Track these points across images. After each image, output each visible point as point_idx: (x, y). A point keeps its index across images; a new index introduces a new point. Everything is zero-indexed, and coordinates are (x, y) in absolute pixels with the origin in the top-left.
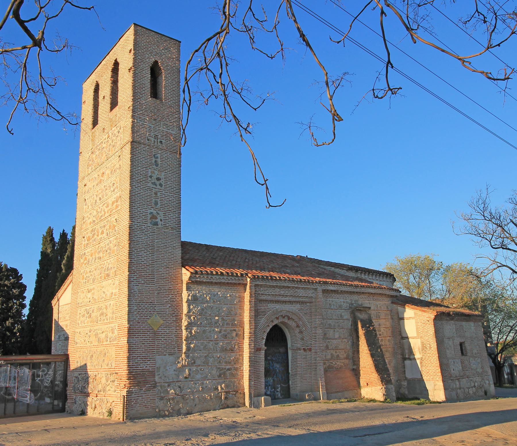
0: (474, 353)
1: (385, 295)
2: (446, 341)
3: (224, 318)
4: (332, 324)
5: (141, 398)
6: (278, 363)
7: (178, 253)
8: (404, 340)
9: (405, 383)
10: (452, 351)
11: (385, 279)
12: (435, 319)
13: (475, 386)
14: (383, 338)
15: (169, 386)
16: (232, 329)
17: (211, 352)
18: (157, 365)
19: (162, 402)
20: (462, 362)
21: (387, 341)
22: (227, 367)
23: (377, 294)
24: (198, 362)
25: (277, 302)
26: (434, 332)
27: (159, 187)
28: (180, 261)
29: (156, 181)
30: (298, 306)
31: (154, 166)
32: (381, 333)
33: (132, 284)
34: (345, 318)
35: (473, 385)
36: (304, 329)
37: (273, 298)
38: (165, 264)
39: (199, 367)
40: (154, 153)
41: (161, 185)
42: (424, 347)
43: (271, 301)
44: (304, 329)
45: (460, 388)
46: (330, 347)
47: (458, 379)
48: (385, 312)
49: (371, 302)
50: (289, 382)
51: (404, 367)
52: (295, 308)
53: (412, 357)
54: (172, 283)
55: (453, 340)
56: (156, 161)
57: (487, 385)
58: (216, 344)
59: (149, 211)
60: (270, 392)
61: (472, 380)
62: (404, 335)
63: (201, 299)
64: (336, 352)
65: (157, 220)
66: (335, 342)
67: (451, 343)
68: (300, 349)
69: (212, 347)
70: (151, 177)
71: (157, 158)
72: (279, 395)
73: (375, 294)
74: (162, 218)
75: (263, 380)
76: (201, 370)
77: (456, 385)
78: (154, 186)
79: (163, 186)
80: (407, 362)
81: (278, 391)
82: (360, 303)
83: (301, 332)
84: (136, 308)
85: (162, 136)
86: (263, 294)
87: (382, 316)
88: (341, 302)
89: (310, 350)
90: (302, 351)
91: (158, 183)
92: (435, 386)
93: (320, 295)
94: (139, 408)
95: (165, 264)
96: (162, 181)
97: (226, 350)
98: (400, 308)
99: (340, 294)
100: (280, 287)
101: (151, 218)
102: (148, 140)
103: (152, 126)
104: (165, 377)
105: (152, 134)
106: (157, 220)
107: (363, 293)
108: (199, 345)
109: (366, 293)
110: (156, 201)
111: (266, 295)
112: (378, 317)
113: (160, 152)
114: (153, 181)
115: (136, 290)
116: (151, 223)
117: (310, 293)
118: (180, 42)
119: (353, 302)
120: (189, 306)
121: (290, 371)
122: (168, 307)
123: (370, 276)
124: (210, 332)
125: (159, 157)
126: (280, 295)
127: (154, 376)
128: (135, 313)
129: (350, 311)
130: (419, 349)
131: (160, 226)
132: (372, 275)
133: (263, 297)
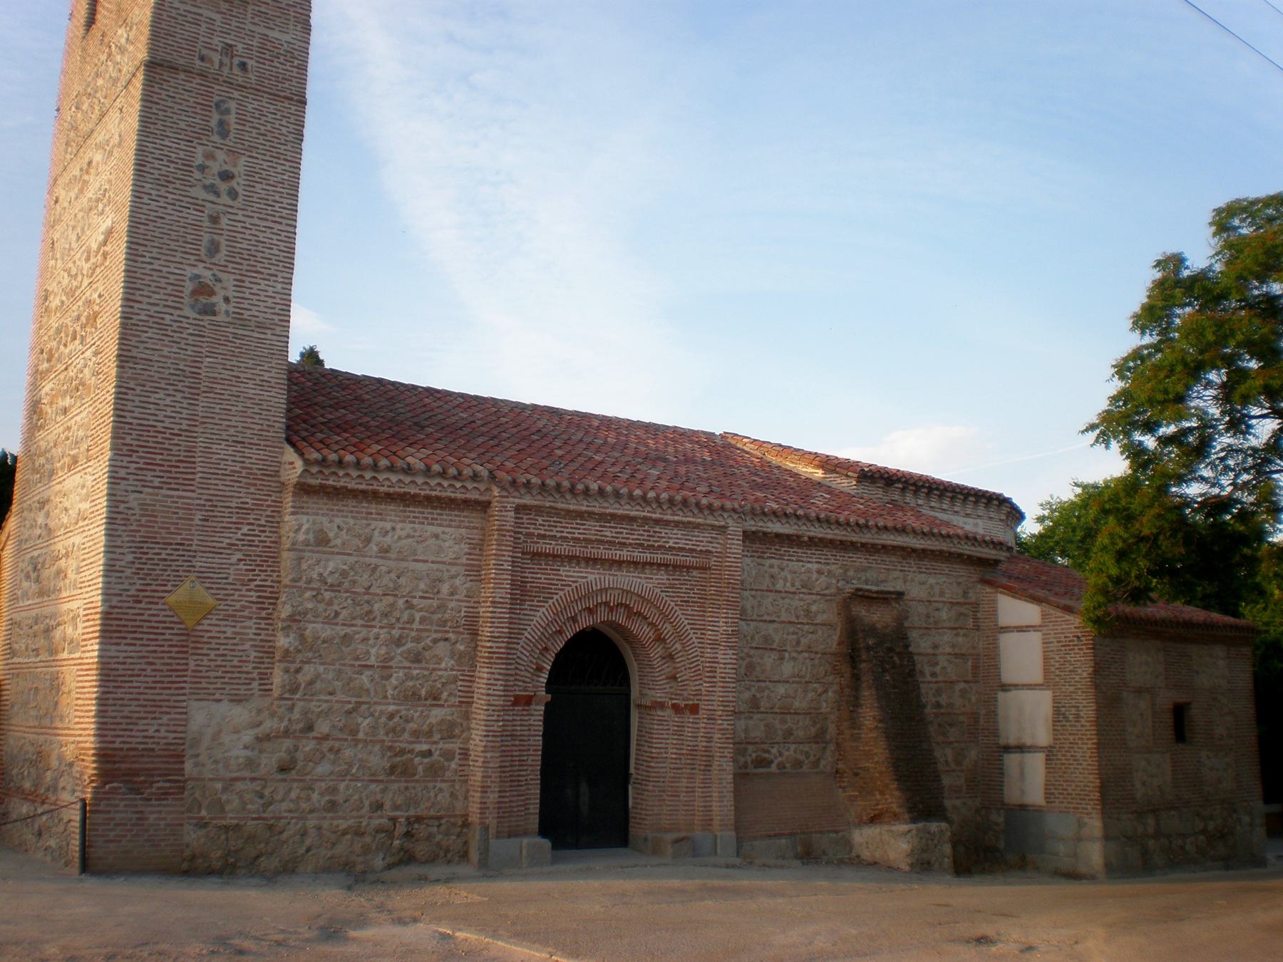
3: (415, 601)
4: (777, 638)
7: (277, 400)
16: (439, 635)
24: (323, 727)
25: (592, 561)
27: (225, 199)
29: (218, 181)
30: (662, 577)
31: (216, 138)
32: (938, 669)
34: (819, 619)
36: (678, 646)
37: (577, 551)
38: (232, 431)
40: (216, 99)
41: (233, 194)
43: (572, 559)
44: (678, 646)
46: (764, 704)
54: (252, 490)
56: (221, 123)
59: (190, 271)
63: (339, 542)
64: (783, 721)
65: (214, 299)
66: (781, 689)
70: (202, 168)
71: (227, 111)
73: (924, 550)
74: (231, 294)
78: (212, 197)
79: (240, 198)
84: (130, 557)
85: (249, 48)
86: (544, 537)
88: (809, 571)
89: (694, 709)
91: (223, 187)
93: (736, 546)
95: (232, 431)
96: (239, 184)
102: (202, 59)
110: (212, 242)
113: (236, 94)
114: (207, 182)
115: (134, 504)
116: (193, 307)
121: (632, 770)
122: (234, 559)
123: (947, 501)
125: (233, 111)
128: (128, 572)
131: (221, 318)
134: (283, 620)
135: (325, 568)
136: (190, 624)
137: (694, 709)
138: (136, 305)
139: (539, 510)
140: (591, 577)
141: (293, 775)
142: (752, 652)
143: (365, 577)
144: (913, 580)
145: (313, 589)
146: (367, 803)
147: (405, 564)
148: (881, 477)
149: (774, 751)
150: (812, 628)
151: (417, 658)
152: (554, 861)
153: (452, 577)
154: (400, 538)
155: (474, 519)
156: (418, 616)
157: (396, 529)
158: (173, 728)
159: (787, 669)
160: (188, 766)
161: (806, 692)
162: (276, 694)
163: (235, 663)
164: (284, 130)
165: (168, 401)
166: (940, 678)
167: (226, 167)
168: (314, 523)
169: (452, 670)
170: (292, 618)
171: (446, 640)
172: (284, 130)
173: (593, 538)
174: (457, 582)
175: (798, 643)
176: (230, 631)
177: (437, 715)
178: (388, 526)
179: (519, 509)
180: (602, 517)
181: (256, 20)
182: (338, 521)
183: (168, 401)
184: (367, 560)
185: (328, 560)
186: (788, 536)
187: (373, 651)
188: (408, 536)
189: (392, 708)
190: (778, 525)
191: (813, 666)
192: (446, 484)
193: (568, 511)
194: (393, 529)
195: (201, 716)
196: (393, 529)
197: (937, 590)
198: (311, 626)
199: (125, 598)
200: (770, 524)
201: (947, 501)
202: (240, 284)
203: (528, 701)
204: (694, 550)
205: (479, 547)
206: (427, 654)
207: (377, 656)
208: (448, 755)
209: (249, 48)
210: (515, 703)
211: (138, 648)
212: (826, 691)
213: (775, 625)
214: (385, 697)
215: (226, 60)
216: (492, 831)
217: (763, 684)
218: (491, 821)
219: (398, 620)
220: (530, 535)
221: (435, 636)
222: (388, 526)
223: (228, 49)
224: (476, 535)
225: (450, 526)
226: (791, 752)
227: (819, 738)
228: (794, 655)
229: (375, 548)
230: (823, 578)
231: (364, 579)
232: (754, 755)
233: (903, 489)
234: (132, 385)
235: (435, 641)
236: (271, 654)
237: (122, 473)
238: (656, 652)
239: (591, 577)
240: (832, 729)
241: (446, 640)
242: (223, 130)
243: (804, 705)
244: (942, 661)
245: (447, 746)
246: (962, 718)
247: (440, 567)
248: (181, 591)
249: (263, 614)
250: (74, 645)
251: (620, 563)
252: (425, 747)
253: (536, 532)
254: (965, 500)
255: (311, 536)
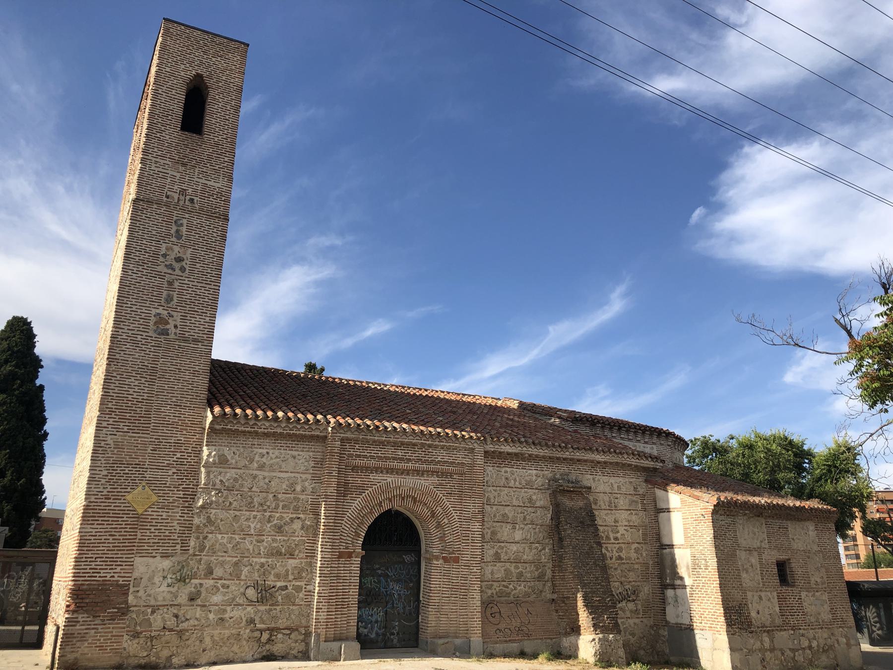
0: (813, 582)
1: (630, 465)
2: (742, 555)
3: (280, 496)
4: (510, 515)
5: (93, 631)
6: (398, 581)
7: (202, 382)
8: (665, 551)
9: (665, 633)
10: (754, 574)
11: (655, 439)
12: (715, 512)
13: (810, 647)
14: (623, 546)
15: (153, 612)
16: (294, 516)
17: (246, 555)
18: (136, 574)
19: (136, 641)
20: (781, 599)
21: (633, 551)
22: (279, 584)
23: (611, 463)
24: (218, 572)
25: (390, 471)
26: (712, 536)
27: (178, 272)
28: (204, 395)
29: (174, 263)
30: (435, 479)
31: (174, 239)
32: (619, 535)
33: (104, 432)
34: (538, 504)
35: (806, 644)
36: (446, 521)
37: (381, 464)
38: (174, 399)
39: (220, 582)
40: (175, 218)
41: (183, 269)
42: (695, 566)
43: (377, 470)
44: (446, 521)
45: (772, 650)
46: (503, 557)
47: (768, 632)
48: (630, 497)
49: (598, 477)
50: (418, 618)
51: (664, 601)
52: (426, 483)
53: (678, 582)
54: (184, 432)
55: (760, 555)
56: (177, 231)
57: (844, 646)
58: (258, 542)
59: (154, 312)
60: (377, 634)
61: (803, 635)
62: (666, 541)
63: (234, 461)
64: (517, 568)
65: (168, 327)
66: (514, 548)
67: (754, 560)
68: (437, 558)
69: (251, 548)
70: (165, 256)
71: (182, 225)
72: (395, 641)
73: (605, 463)
74: (178, 324)
75: (354, 611)
76: (223, 586)
77: (761, 641)
78: (170, 271)
79: (187, 271)
80: (670, 593)
81: (393, 634)
82: (573, 477)
83: (439, 526)
84: (105, 473)
85: (195, 191)
86: (359, 456)
87: (622, 503)
88: (530, 475)
89: (456, 560)
90: (441, 561)
91: (177, 266)
92: (714, 641)
93: (480, 460)
94: (86, 651)
95: (174, 399)
96: (186, 264)
97: (281, 554)
98: (659, 493)
99: (529, 460)
100: (395, 445)
101: (156, 323)
102: (167, 197)
103: (178, 175)
104: (150, 596)
105: (176, 187)
106: (168, 327)
107: (578, 460)
108: (225, 541)
109: (586, 461)
110: (169, 295)
111: (365, 457)
112: (613, 507)
113: (187, 216)
114: (167, 263)
115: (110, 442)
116: (155, 331)
117: (460, 457)
118: (248, 45)
119: (558, 476)
120: (208, 473)
121: (421, 599)
122: (170, 473)
123: (632, 434)
124: (248, 519)
125: (185, 225)
126: (394, 459)
127: (126, 594)
128: (103, 481)
129: (549, 492)
130: (688, 568)
131: (172, 336)
132: (635, 433)
133: (358, 462)
134: (198, 508)
135: (224, 477)
136: (140, 511)
137: (456, 560)
138: (121, 331)
139: (356, 441)
140: (389, 480)
141: (199, 602)
142: (495, 524)
143: (249, 481)
144: (599, 480)
145: (217, 489)
146: (244, 619)
147: (274, 474)
148: (598, 422)
149: (511, 586)
150: (532, 510)
151: (279, 529)
152: (363, 657)
154: (271, 459)
155: (319, 447)
156: (281, 504)
157: (270, 453)
158: (122, 575)
159: (518, 535)
160: (131, 598)
161: (531, 549)
162: (191, 552)
163: (167, 534)
164: (215, 235)
165: (137, 383)
166: (620, 541)
167: (179, 255)
168: (219, 450)
170: (203, 507)
172: (215, 235)
174: (307, 484)
175: (525, 519)
176: (164, 514)
177: (292, 563)
178: (264, 451)
179: (342, 440)
181: (201, 176)
182: (233, 449)
183: (137, 383)
184: (251, 472)
185: (226, 473)
186: (516, 454)
187: (252, 526)
188: (277, 457)
189: (263, 560)
190: (508, 447)
191: (535, 533)
192: (299, 427)
193: (374, 441)
194: (268, 453)
195: (142, 566)
196: (268, 453)
197: (615, 486)
198: (214, 511)
199: (99, 497)
200: (503, 447)
201: (632, 434)
202: (184, 318)
203: (350, 555)
205: (319, 463)
206: (286, 528)
207: (255, 528)
208: (298, 589)
209: (195, 191)
210: (340, 557)
211: (105, 526)
212: (544, 549)
213: (509, 508)
214: (260, 554)
215: (182, 198)
216: (322, 638)
217: (502, 544)
218: (322, 631)
219: (269, 507)
220: (351, 456)
221: (291, 516)
222: (264, 451)
223: (183, 192)
224: (319, 456)
225: (302, 451)
226: (521, 588)
227: (541, 577)
228: (522, 526)
229: (256, 465)
230: (539, 479)
231: (247, 484)
232: (497, 589)
233: (602, 427)
234: (115, 374)
235: (292, 520)
236: (190, 528)
237: (105, 424)
238: (432, 526)
239: (389, 480)
240: (549, 573)
242: (178, 235)
243: (530, 558)
244: (622, 530)
245: (297, 583)
246: (636, 566)
247: (296, 475)
248: (136, 492)
249: (187, 504)
250: (726, 498)
252: (284, 584)
254: (644, 433)
255: (217, 459)
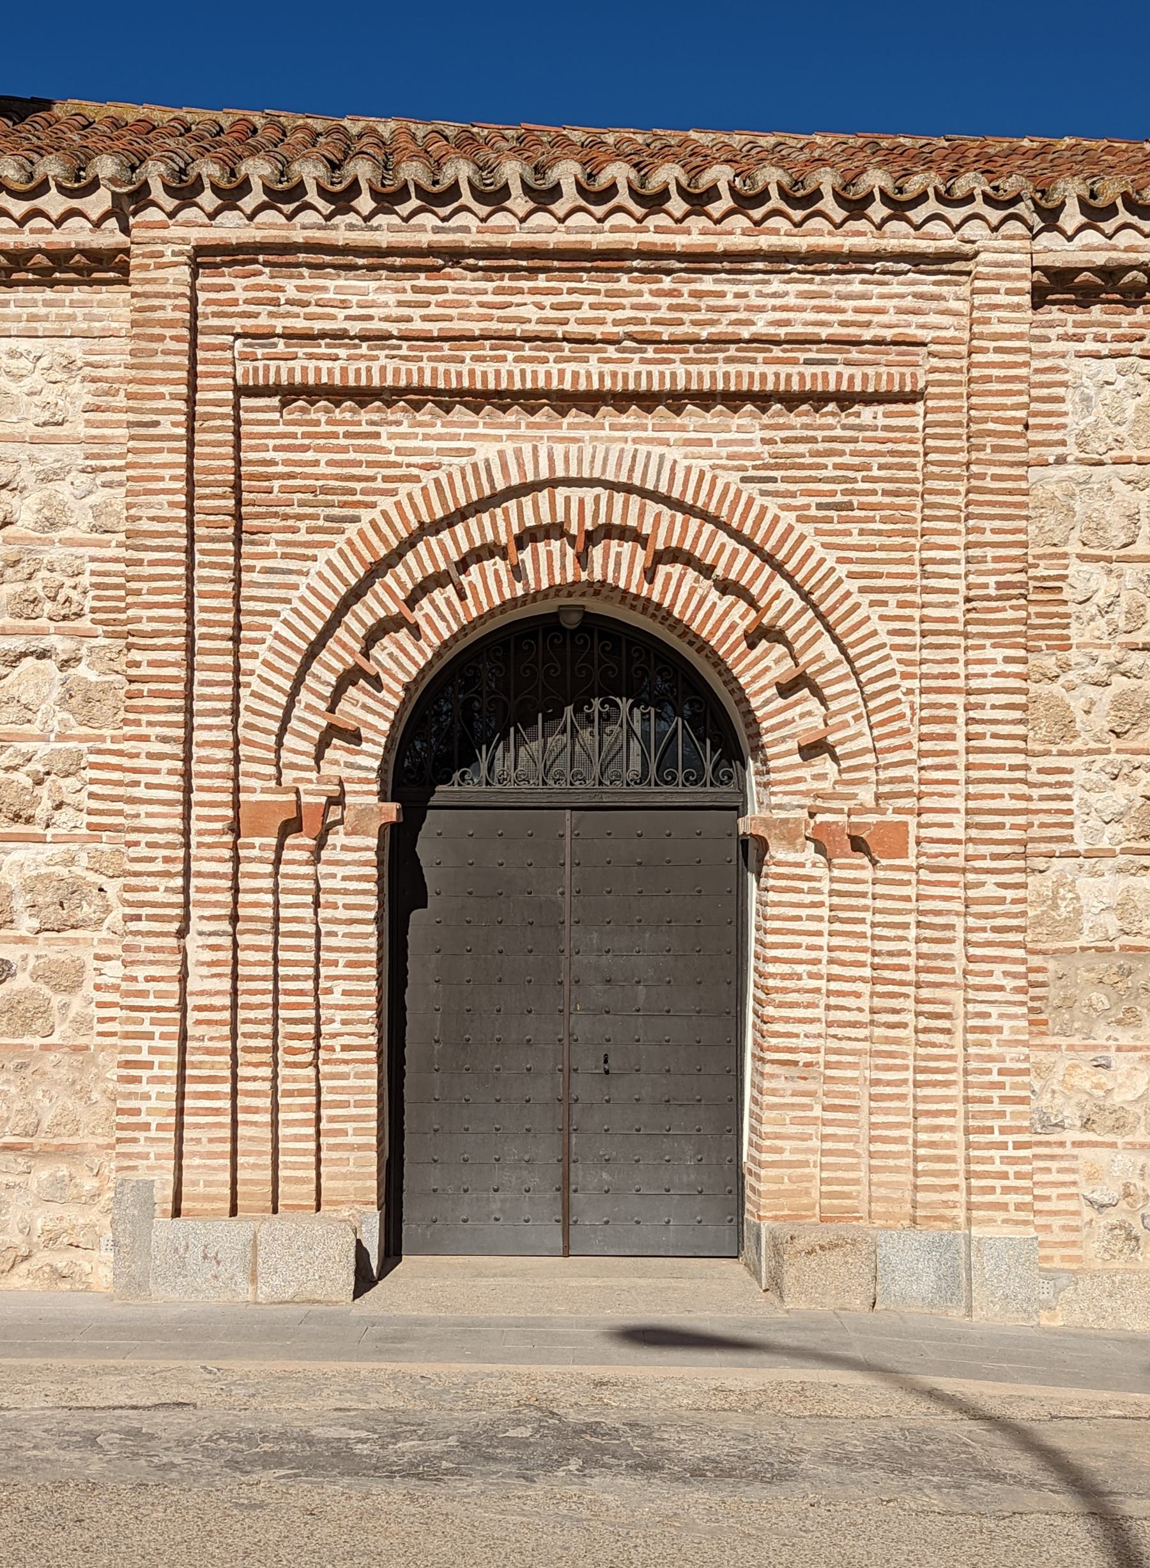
30: (746, 429)
93: (1011, 314)
153: (46, 478)
169: (61, 737)
171: (43, 655)
173: (476, 328)
174: (64, 490)
179: (205, 258)
180: (495, 260)
204: (849, 507)
241: (43, 655)
251: (590, 401)
253: (279, 325)
